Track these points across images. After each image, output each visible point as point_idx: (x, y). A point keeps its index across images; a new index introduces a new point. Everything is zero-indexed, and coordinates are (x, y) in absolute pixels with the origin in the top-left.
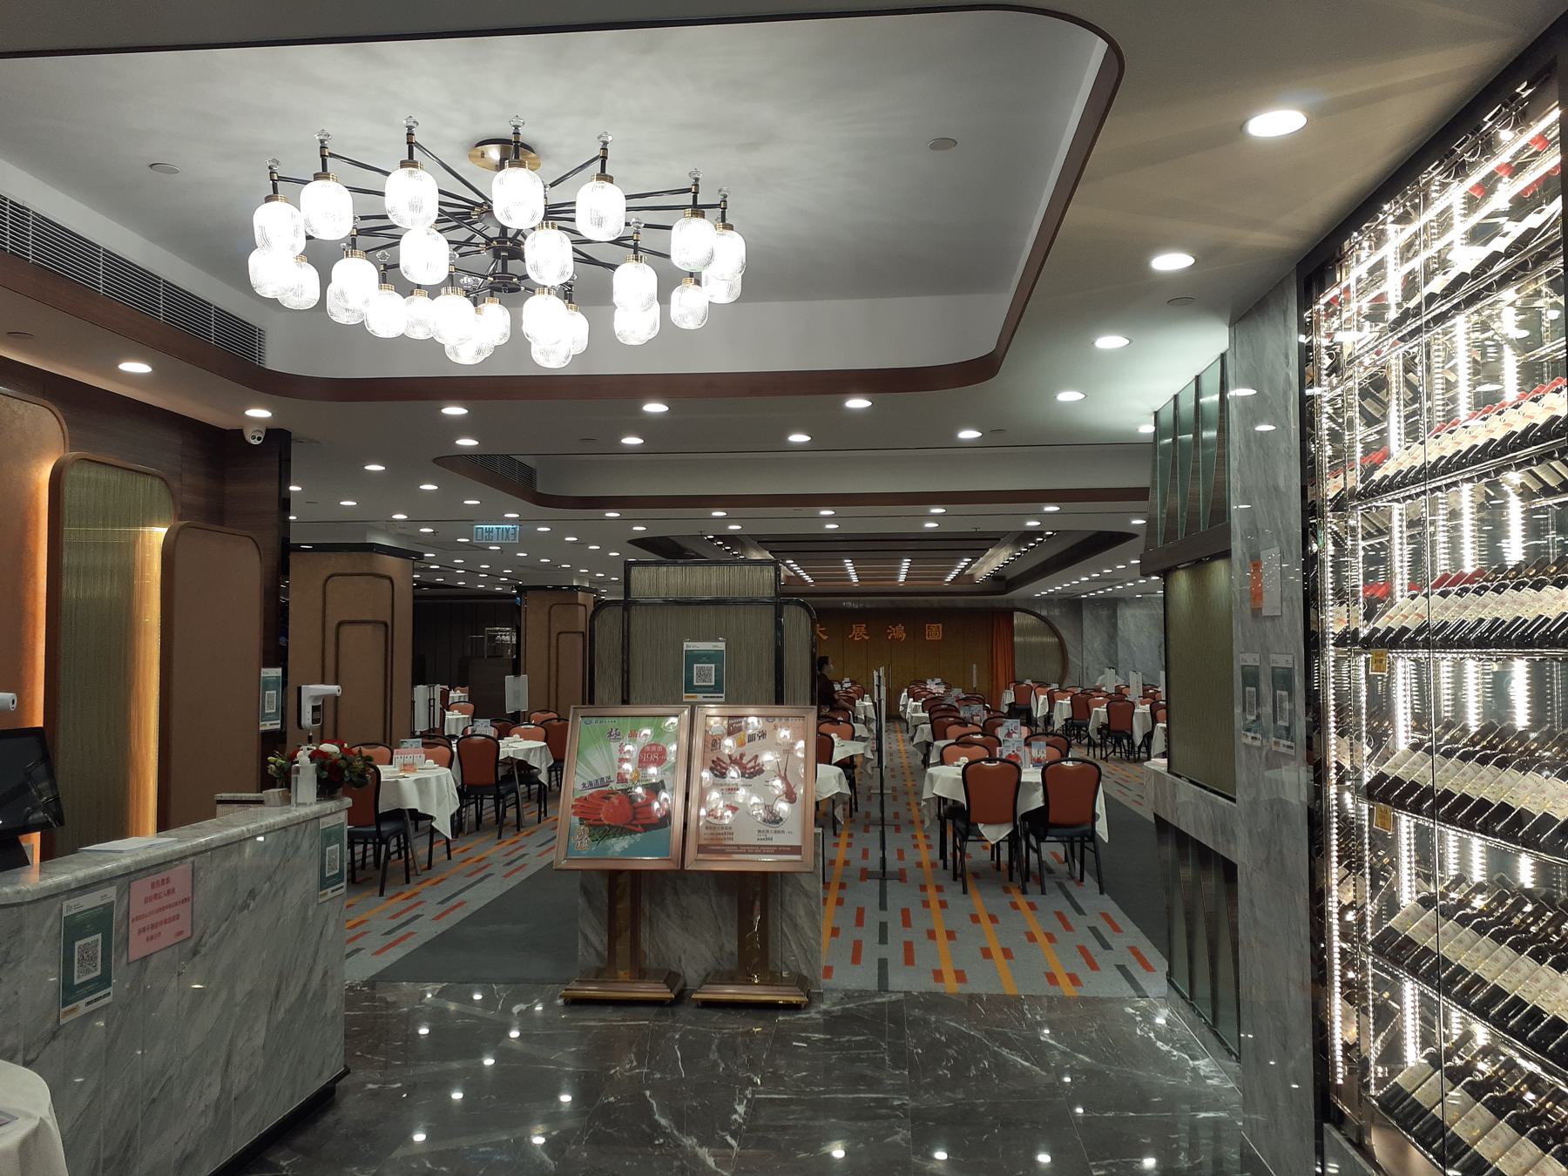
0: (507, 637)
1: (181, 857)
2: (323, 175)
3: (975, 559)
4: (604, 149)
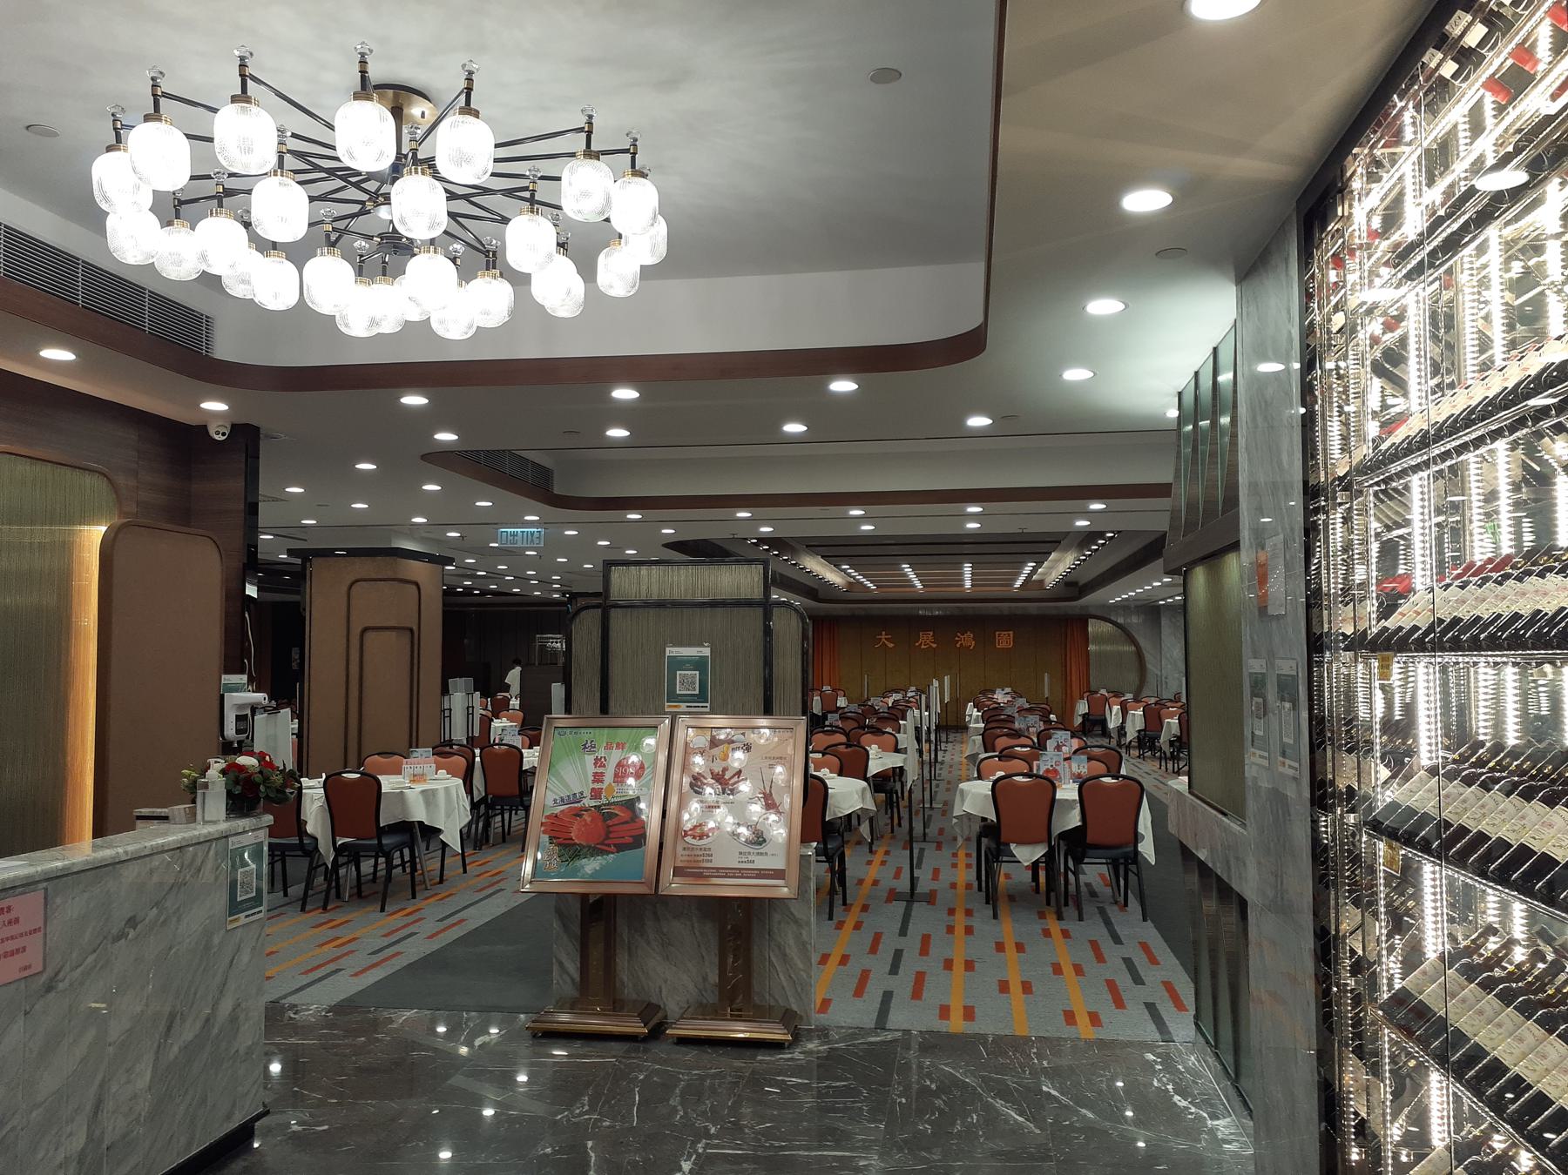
0: (557, 644)
1: (28, 884)
2: (154, 115)
3: (1039, 564)
4: (470, 80)
